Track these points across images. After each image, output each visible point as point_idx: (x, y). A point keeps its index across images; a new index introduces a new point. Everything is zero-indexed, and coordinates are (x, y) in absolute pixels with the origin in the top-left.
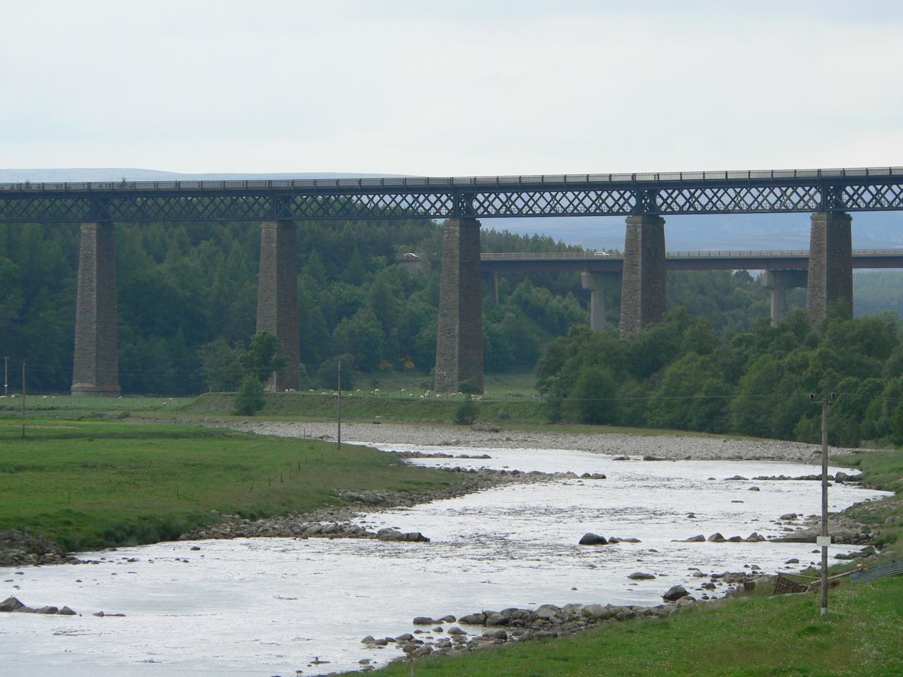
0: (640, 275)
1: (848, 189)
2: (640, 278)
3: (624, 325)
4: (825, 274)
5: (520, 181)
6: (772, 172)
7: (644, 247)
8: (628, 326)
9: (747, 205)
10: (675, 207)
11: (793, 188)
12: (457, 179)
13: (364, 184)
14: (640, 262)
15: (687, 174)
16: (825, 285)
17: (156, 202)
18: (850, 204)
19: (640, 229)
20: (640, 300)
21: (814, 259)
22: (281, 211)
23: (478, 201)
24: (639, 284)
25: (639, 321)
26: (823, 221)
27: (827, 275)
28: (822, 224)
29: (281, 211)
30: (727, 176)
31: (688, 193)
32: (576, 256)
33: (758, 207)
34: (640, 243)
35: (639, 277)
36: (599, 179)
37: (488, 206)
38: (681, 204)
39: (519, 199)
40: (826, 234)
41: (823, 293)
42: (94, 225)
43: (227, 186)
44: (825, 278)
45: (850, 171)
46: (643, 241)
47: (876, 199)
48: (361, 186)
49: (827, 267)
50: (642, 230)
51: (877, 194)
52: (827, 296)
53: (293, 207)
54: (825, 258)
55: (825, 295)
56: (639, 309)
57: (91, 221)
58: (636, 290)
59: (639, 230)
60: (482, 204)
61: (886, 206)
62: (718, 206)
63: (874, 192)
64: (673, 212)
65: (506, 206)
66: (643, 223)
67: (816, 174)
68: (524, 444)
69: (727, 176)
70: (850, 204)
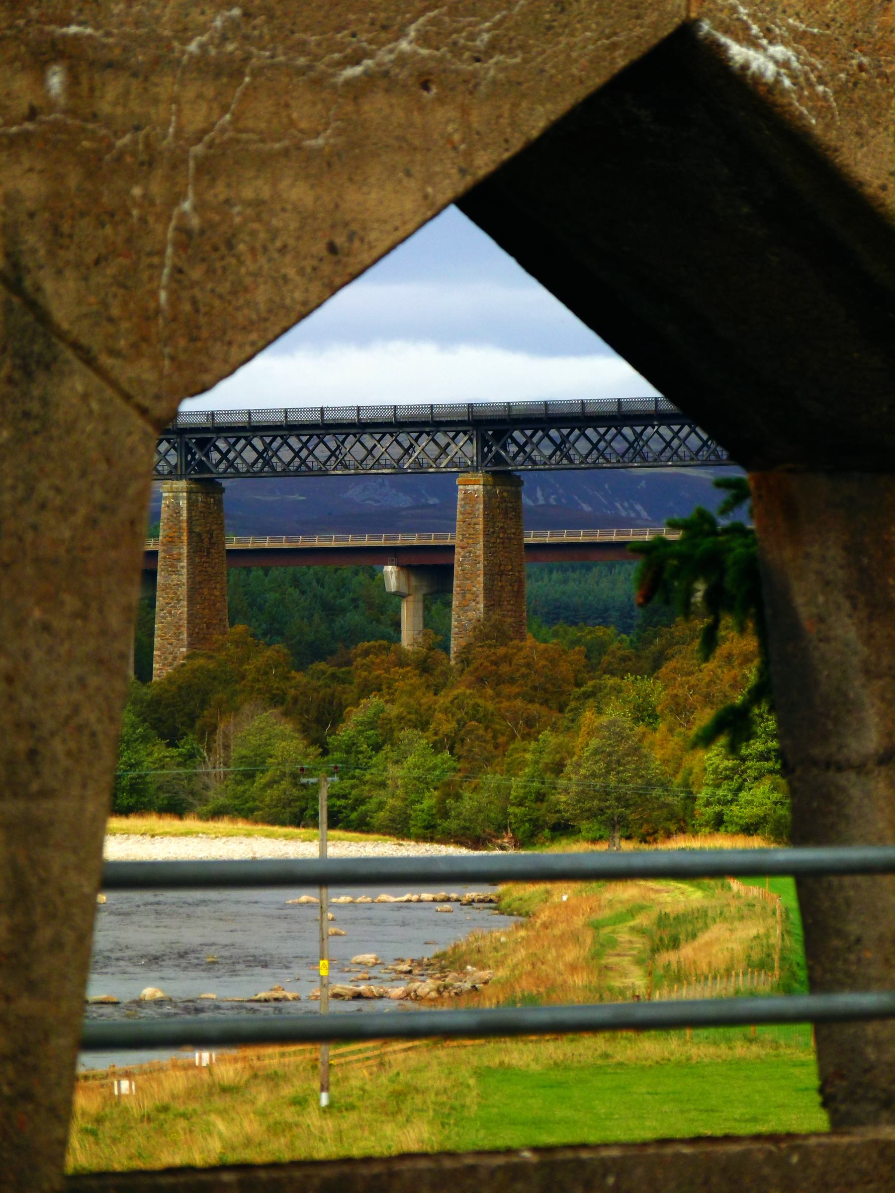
0: (185, 576)
1: (517, 434)
2: (185, 581)
3: (160, 656)
4: (482, 572)
5: (432, 412)
6: (359, 409)
7: (190, 531)
8: (166, 659)
9: (581, 455)
10: (240, 466)
11: (616, 429)
12: (439, 406)
13: (219, 420)
14: (185, 555)
15: (258, 412)
16: (481, 589)
17: (433, 440)
18: (222, 467)
19: (185, 502)
20: (185, 616)
21: (462, 548)
22: (490, 455)
23: (219, 451)
24: (183, 591)
25: (184, 650)
26: (476, 487)
27: (485, 574)
28: (476, 491)
29: (490, 455)
30: (322, 415)
31: (595, 434)
32: (617, 535)
33: (300, 466)
34: (185, 525)
35: (184, 579)
36: (640, 407)
37: (235, 459)
38: (287, 459)
39: (321, 445)
40: (482, 506)
41: (478, 603)
42: (182, 484)
43: (589, 409)
44: (481, 579)
45: (518, 404)
46: (190, 520)
47: (264, 459)
48: (359, 420)
49: (485, 560)
50: (188, 503)
51: (636, 440)
52: (485, 606)
53: (215, 456)
54: (481, 545)
55: (481, 606)
56: (184, 630)
57: (179, 478)
58: (179, 601)
59: (183, 503)
60: (224, 456)
61: (279, 469)
62: (310, 464)
63: (631, 438)
64: (238, 474)
65: (264, 459)
66: (189, 492)
67: (615, 408)
68: (367, 860)
69: (322, 415)
70: (222, 467)
